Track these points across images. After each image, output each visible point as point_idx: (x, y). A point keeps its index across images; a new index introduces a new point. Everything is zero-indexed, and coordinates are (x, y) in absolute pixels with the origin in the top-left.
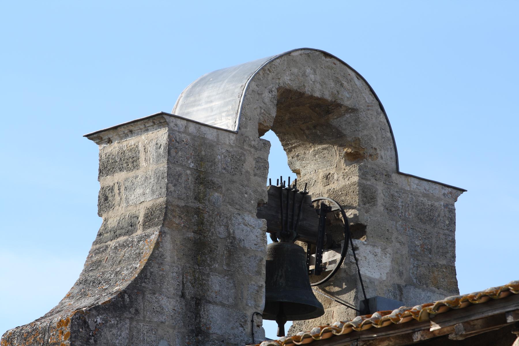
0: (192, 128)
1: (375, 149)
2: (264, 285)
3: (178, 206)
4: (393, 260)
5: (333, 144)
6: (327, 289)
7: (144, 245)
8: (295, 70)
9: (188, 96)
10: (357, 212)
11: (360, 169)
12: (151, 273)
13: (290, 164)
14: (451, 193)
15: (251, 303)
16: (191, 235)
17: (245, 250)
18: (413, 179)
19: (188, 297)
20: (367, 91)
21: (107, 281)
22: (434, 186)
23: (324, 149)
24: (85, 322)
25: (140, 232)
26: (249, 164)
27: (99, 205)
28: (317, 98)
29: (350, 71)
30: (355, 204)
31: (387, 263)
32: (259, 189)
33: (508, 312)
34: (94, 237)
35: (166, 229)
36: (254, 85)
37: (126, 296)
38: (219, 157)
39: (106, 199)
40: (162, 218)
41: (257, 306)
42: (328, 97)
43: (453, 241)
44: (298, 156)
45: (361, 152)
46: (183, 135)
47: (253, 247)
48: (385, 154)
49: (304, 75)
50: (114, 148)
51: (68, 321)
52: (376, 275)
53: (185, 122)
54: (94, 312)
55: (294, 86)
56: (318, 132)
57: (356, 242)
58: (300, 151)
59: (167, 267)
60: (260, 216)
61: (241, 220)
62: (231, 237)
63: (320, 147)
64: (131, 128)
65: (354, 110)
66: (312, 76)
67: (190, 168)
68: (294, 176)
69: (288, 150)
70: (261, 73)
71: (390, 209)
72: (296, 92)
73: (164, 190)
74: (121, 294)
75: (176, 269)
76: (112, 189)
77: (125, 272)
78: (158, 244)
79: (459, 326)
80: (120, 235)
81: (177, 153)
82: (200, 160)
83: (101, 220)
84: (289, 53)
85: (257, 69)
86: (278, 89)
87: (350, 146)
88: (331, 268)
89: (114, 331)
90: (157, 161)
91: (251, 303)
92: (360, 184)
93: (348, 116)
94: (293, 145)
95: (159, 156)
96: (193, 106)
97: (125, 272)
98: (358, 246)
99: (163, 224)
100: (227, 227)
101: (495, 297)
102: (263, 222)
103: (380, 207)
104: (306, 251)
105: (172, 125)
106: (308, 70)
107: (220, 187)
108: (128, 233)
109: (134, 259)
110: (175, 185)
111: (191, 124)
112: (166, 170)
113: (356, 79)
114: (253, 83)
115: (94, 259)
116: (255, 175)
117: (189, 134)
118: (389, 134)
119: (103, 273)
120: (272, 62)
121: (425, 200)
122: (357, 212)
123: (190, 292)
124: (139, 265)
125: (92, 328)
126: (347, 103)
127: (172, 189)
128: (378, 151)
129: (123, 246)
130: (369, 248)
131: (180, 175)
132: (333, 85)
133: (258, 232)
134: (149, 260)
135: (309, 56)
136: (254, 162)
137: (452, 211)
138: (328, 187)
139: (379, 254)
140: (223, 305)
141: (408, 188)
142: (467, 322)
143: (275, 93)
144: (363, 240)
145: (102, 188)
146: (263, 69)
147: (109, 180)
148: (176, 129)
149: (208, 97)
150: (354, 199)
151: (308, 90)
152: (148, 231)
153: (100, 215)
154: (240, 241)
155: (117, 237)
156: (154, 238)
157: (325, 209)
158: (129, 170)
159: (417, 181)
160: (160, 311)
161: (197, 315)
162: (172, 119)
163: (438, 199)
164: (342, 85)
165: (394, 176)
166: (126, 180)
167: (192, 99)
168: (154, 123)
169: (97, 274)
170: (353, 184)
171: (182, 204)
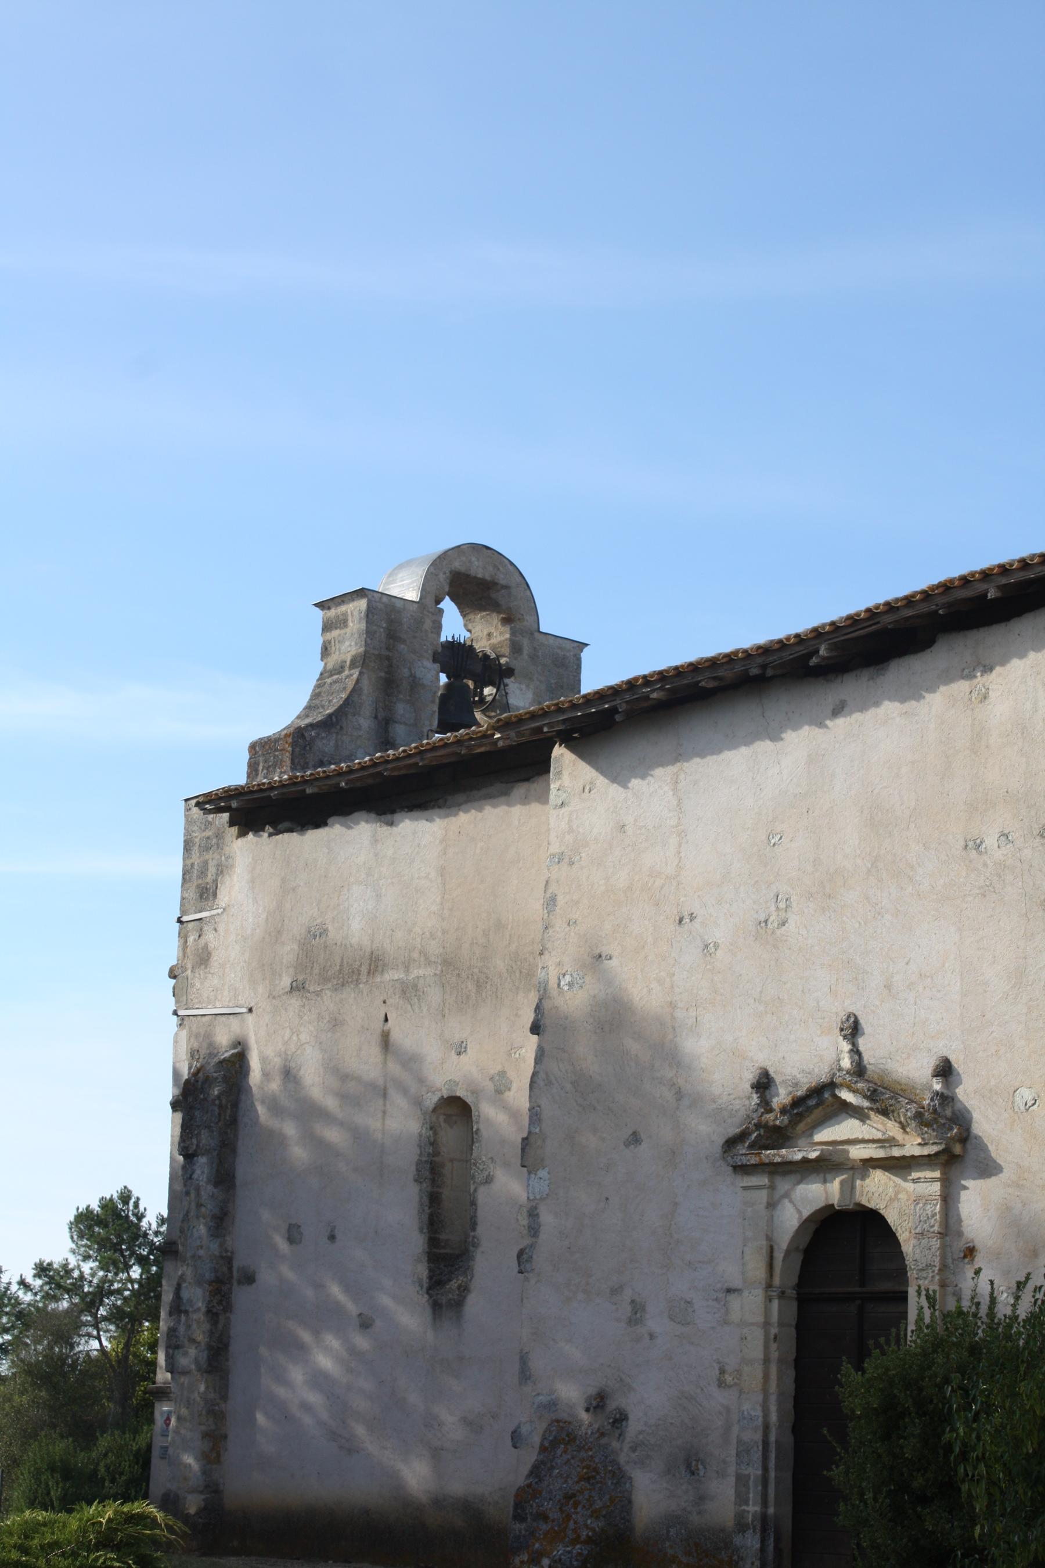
0: (385, 599)
1: (523, 615)
2: (437, 710)
3: (374, 654)
4: (534, 694)
5: (493, 611)
6: (487, 714)
7: (349, 682)
8: (464, 559)
9: (389, 577)
10: (508, 660)
11: (511, 629)
12: (353, 701)
13: (465, 626)
14: (578, 646)
15: (427, 723)
16: (383, 674)
17: (423, 686)
18: (550, 636)
19: (380, 717)
20: (518, 573)
21: (323, 707)
22: (566, 641)
23: (487, 615)
24: (303, 735)
25: (347, 672)
26: (428, 624)
27: (322, 654)
28: (480, 579)
29: (505, 560)
30: (507, 654)
31: (530, 695)
32: (435, 643)
33: (544, 725)
34: (317, 676)
35: (364, 670)
36: (432, 569)
37: (334, 717)
38: (405, 620)
39: (326, 649)
40: (361, 662)
41: (431, 725)
42: (488, 578)
43: (580, 681)
44: (470, 620)
45: (512, 617)
46: (378, 604)
47: (429, 684)
48: (529, 619)
49: (470, 562)
50: (332, 613)
51: (290, 734)
52: (521, 704)
53: (380, 595)
54: (310, 728)
55: (463, 569)
56: (484, 604)
57: (506, 681)
58: (471, 616)
59: (364, 697)
60: (435, 661)
61: (420, 664)
62: (413, 676)
63: (485, 613)
64: (343, 599)
65: (507, 587)
66: (476, 563)
67: (383, 628)
68: (468, 635)
69: (464, 615)
70: (438, 560)
71: (533, 657)
72: (464, 574)
73: (363, 643)
74: (330, 716)
75: (371, 699)
76: (330, 642)
77: (335, 701)
78: (358, 681)
79: (512, 734)
80: (334, 674)
81: (373, 616)
82: (390, 621)
83: (322, 664)
84: (459, 547)
85: (435, 557)
86: (451, 572)
87: (504, 613)
88: (489, 699)
89: (324, 742)
90: (360, 622)
91: (427, 723)
92: (510, 640)
93: (503, 591)
94: (936, 591)
95: (361, 618)
96: (392, 584)
97: (335, 701)
98: (508, 683)
99: (362, 667)
100: (410, 669)
101: (535, 714)
102: (437, 666)
103: (525, 656)
104: (472, 687)
105: (370, 596)
106: (473, 559)
107: (405, 641)
108: (340, 673)
109: (342, 691)
110: (371, 639)
111: (384, 596)
112: (365, 628)
113: (509, 565)
114: (432, 567)
115: (317, 691)
116: (432, 632)
117: (383, 603)
118: (533, 605)
119: (321, 701)
120: (446, 553)
121: (559, 651)
122: (508, 660)
123: (381, 715)
124: (344, 696)
125: (308, 739)
126: (503, 582)
127: (369, 641)
128: (525, 616)
129: (335, 682)
130: (516, 685)
131: (375, 632)
132: (491, 569)
133: (433, 673)
134: (351, 692)
135: (474, 548)
136: (431, 624)
137: (579, 660)
138: (490, 642)
139: (524, 689)
140: (406, 724)
141: (546, 643)
142: (519, 732)
143: (448, 574)
144: (512, 679)
145: (324, 642)
146: (439, 557)
147: (329, 636)
148: (373, 599)
149: (402, 577)
150: (506, 650)
151: (473, 573)
152: (353, 671)
153: (322, 660)
154: (420, 679)
155: (332, 675)
156: (355, 676)
157: (486, 657)
158: (341, 628)
159: (553, 638)
160: (359, 728)
161: (386, 731)
162: (369, 592)
163: (569, 651)
164: (499, 569)
165: (536, 634)
166: (339, 635)
167: (391, 579)
168: (358, 595)
169: (317, 702)
170: (506, 640)
171: (376, 652)
